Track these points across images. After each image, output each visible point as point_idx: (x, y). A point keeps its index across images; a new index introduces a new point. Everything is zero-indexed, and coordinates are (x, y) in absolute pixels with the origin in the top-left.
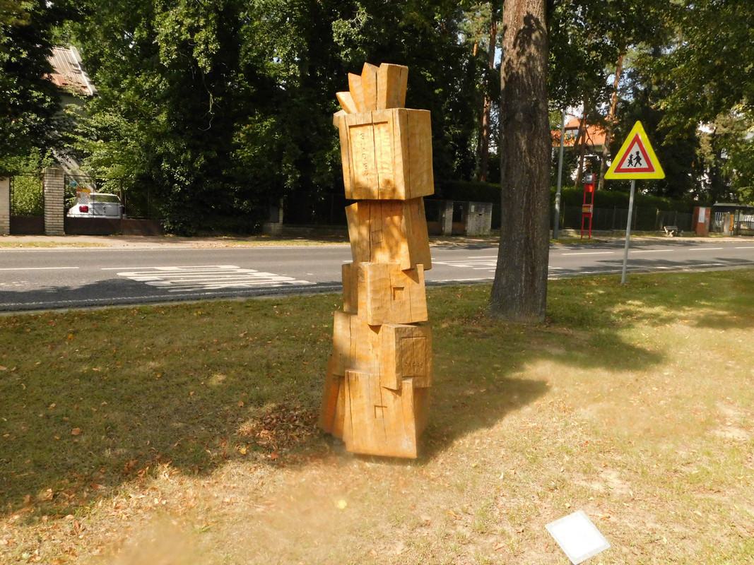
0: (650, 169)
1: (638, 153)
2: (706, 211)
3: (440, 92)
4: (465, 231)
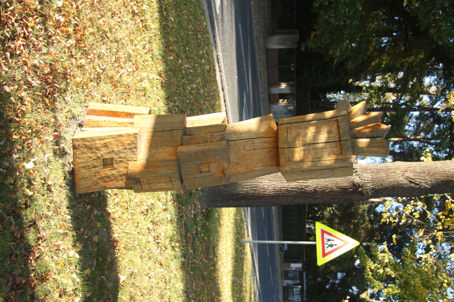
0: (323, 232)
1: (336, 245)
2: (299, 268)
3: (416, 80)
4: (272, 86)
